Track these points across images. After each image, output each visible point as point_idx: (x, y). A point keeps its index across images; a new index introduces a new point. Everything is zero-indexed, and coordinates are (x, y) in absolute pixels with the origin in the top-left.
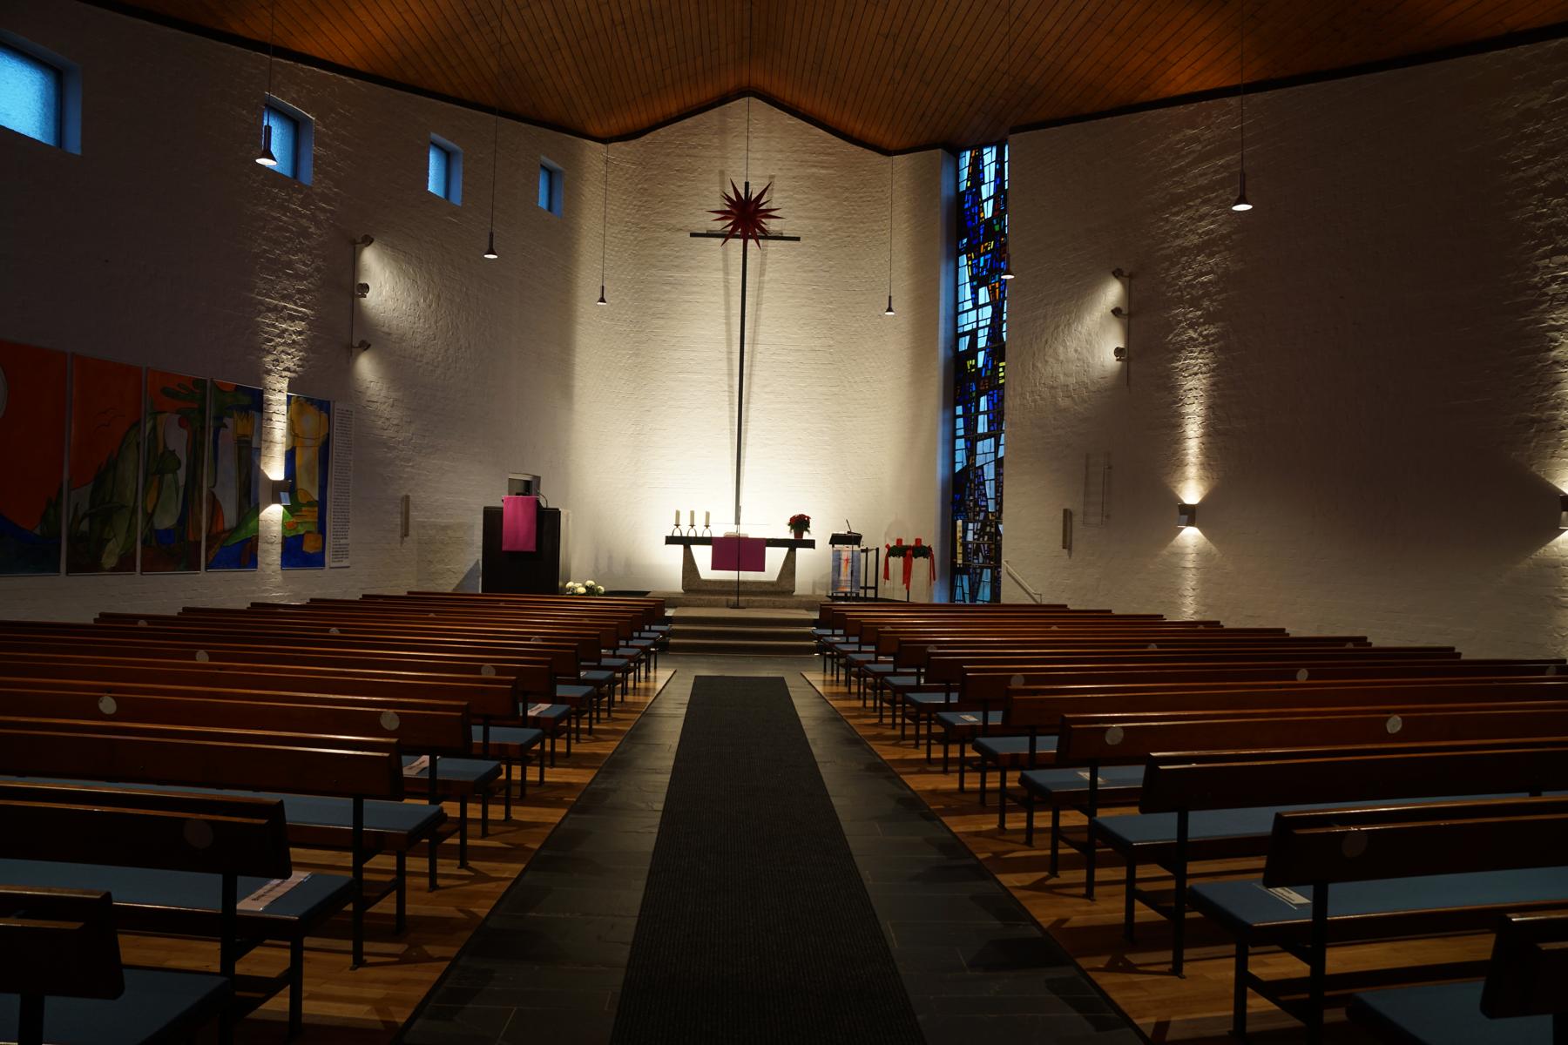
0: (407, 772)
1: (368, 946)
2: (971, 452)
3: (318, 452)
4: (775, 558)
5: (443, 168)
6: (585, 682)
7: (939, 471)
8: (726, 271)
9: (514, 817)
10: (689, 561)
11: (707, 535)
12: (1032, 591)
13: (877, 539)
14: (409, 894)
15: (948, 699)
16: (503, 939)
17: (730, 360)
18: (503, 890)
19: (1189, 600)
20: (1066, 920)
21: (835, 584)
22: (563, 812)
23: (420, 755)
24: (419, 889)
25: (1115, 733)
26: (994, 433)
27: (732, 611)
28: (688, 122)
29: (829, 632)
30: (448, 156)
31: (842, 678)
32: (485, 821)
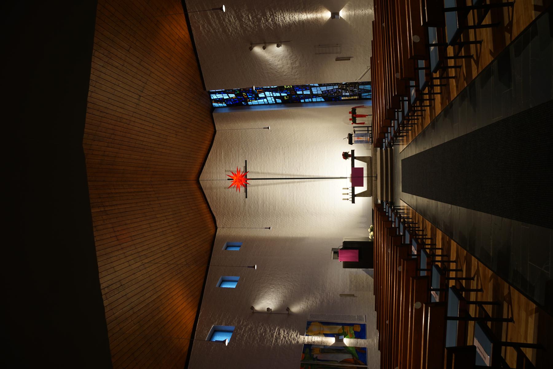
0: (437, 300)
1: (505, 317)
2: (317, 96)
3: (325, 325)
4: (358, 164)
5: (228, 283)
6: (404, 233)
7: (325, 107)
8: (258, 185)
9: (454, 259)
10: (361, 195)
11: (351, 189)
12: (366, 70)
13: (350, 128)
14: (484, 300)
15: (406, 100)
16: (502, 264)
17: (289, 183)
18: (482, 265)
19: (367, 12)
20: (490, 51)
21: (367, 142)
22: (452, 241)
23: (431, 294)
24: (482, 296)
25: (416, 39)
26: (310, 88)
27: (379, 178)
28: (209, 200)
29: (384, 144)
30: (223, 281)
31: (401, 138)
32: (456, 270)
